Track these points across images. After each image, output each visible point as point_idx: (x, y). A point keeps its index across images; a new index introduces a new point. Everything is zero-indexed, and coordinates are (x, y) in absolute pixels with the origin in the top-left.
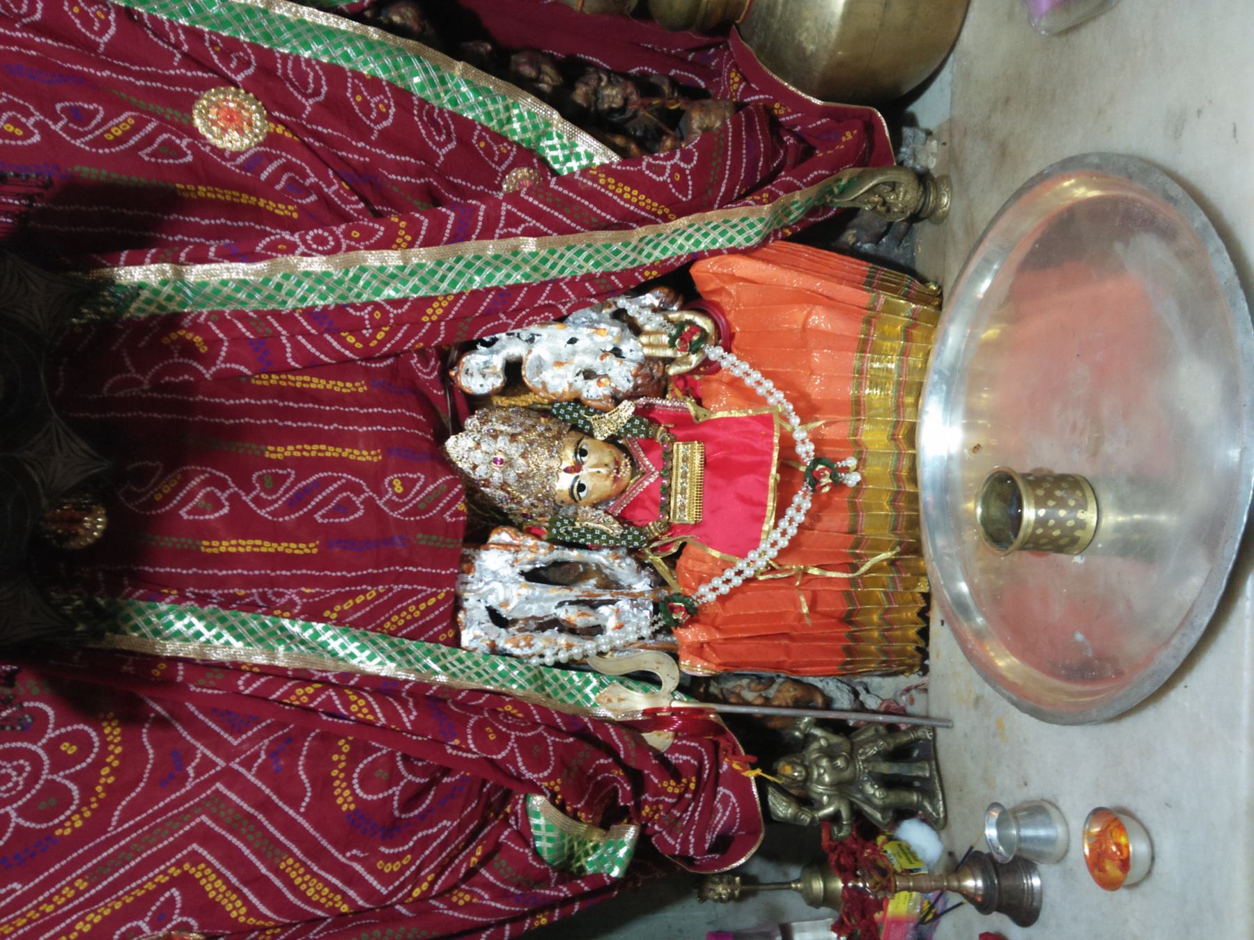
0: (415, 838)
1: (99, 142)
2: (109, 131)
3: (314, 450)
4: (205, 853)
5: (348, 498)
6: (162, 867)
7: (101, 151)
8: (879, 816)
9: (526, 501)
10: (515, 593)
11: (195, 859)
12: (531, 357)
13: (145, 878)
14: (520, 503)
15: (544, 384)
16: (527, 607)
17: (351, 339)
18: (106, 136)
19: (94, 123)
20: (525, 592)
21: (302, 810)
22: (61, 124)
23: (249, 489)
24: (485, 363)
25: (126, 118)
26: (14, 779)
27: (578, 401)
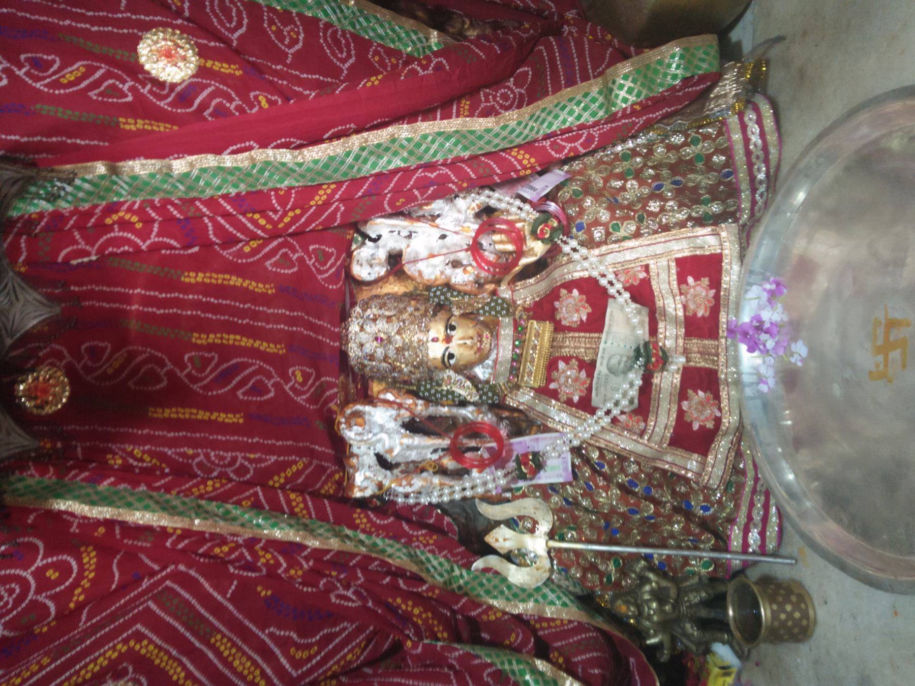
0: (321, 633)
1: (56, 85)
2: (64, 76)
3: (231, 339)
4: (147, 632)
5: (261, 381)
6: (111, 644)
7: (57, 92)
8: (694, 648)
9: (405, 370)
10: (397, 442)
11: (139, 637)
12: (409, 250)
13: (97, 654)
14: (401, 371)
15: (420, 273)
16: (408, 453)
17: (262, 222)
18: (62, 80)
19: (51, 70)
20: (407, 441)
21: (228, 596)
22: (24, 70)
23: (170, 374)
24: (372, 255)
25: (79, 66)
26: (6, 599)
27: (448, 286)
